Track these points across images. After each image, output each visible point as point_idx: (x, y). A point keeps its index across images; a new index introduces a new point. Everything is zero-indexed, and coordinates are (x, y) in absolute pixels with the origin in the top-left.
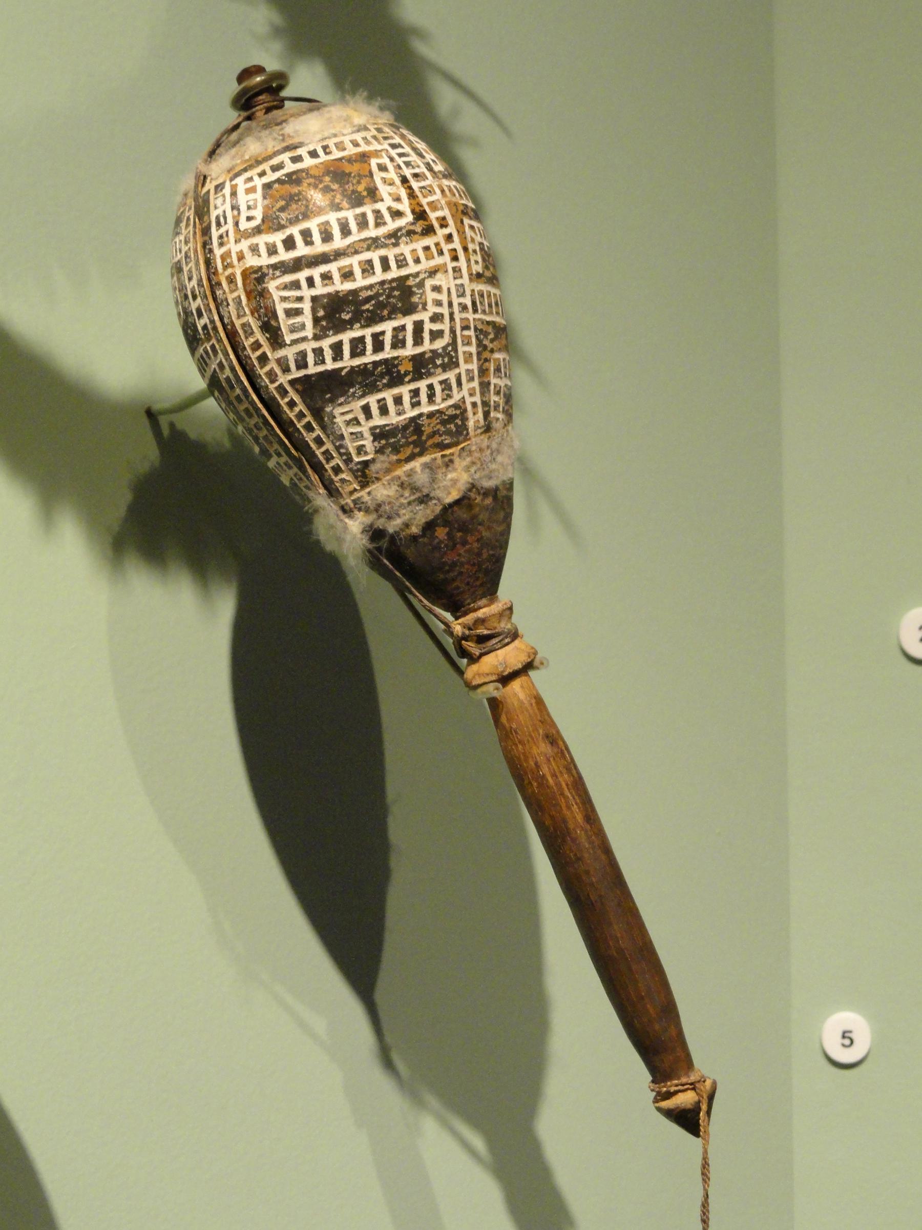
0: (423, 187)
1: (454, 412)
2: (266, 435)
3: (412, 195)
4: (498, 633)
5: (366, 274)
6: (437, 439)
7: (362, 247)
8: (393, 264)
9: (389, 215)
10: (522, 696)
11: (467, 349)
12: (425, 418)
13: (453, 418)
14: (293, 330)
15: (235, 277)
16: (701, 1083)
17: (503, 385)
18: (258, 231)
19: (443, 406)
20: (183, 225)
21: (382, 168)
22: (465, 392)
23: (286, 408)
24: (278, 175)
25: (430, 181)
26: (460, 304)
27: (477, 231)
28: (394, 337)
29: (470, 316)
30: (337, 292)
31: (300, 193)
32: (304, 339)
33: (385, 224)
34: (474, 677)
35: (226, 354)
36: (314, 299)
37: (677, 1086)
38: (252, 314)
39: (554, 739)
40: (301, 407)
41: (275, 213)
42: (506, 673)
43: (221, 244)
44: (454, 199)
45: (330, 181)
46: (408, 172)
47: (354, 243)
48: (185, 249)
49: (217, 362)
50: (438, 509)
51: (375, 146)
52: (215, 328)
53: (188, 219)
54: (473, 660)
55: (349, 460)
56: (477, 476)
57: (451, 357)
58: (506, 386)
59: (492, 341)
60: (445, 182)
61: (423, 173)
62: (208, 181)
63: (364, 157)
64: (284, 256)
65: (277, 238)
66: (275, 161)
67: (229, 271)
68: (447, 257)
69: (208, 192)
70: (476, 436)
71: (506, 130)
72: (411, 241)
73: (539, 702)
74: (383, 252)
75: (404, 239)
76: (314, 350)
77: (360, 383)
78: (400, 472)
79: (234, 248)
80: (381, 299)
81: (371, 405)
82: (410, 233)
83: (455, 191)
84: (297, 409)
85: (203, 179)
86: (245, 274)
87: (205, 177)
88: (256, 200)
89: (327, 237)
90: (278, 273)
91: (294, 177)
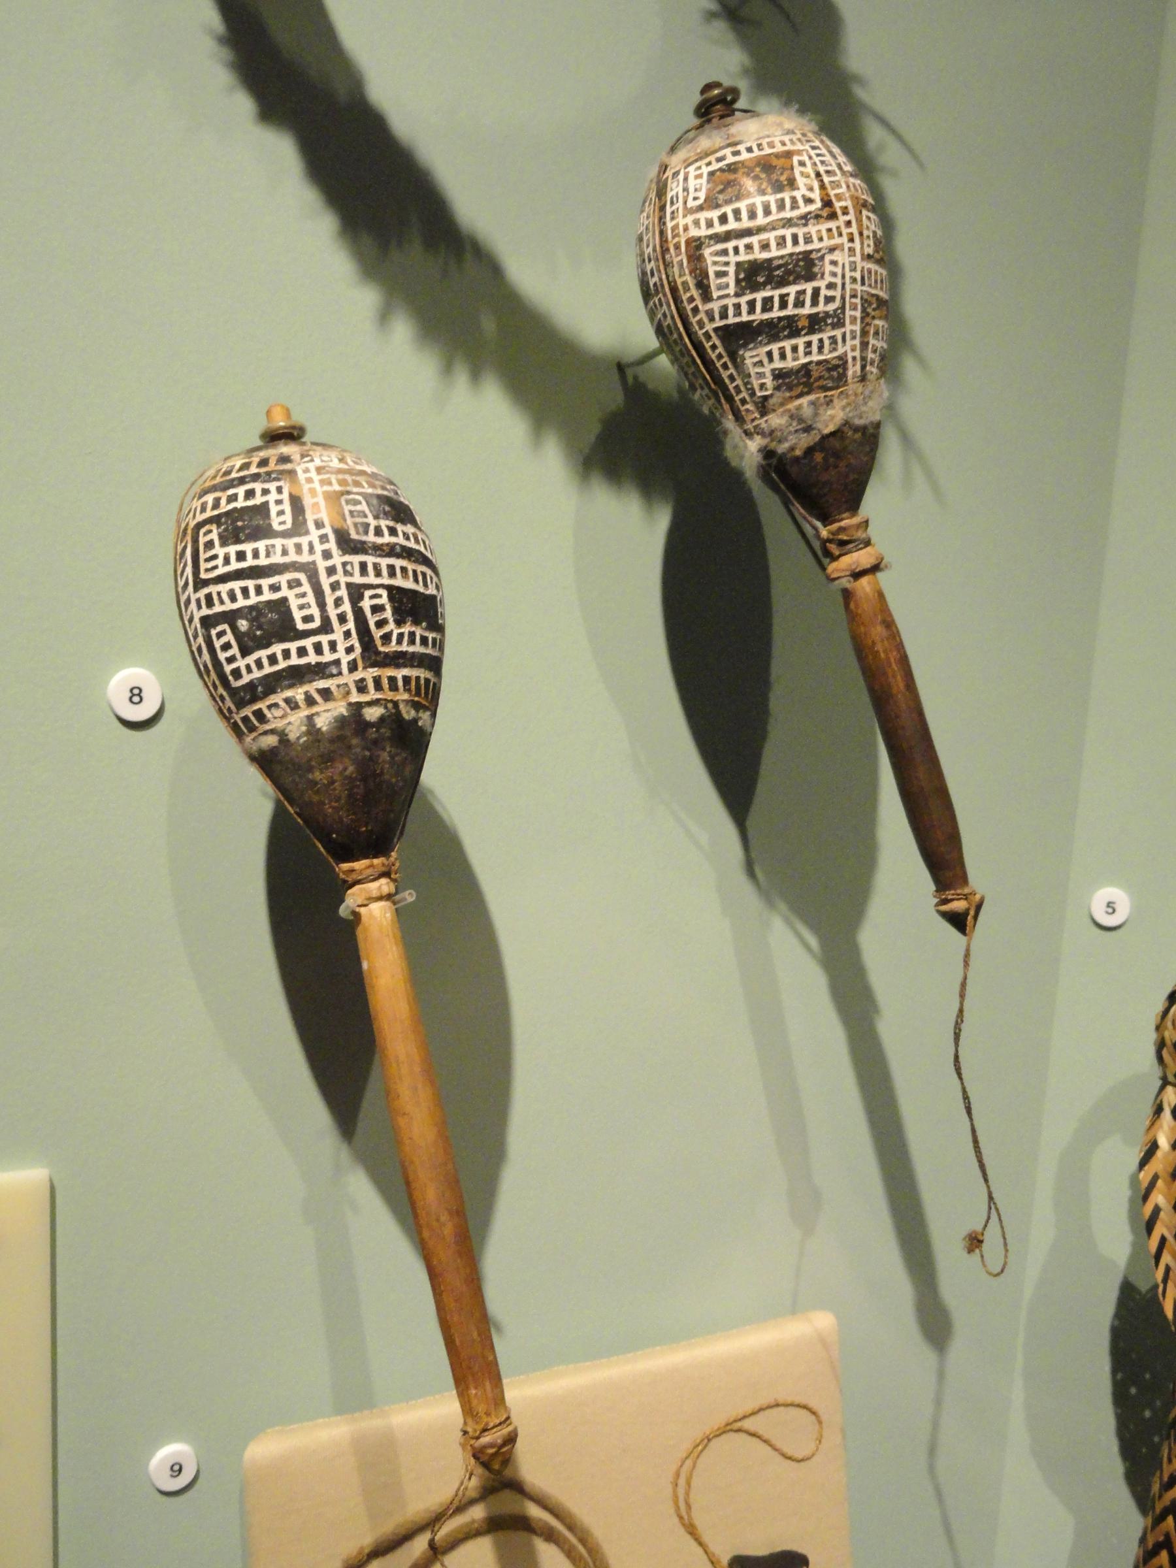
0: (833, 182)
1: (837, 362)
2: (694, 372)
3: (823, 187)
4: (855, 540)
5: (779, 246)
6: (821, 383)
7: (778, 225)
8: (801, 240)
9: (802, 201)
10: (868, 589)
11: (853, 313)
12: (814, 364)
13: (836, 367)
14: (720, 288)
15: (680, 245)
16: (973, 896)
17: (879, 346)
18: (701, 208)
19: (829, 356)
20: (647, 204)
21: (802, 164)
22: (848, 347)
23: (709, 351)
24: (721, 165)
25: (839, 176)
26: (851, 277)
27: (873, 221)
28: (797, 298)
29: (858, 287)
30: (756, 260)
31: (735, 180)
32: (727, 296)
33: (798, 208)
34: (833, 572)
35: (669, 306)
36: (738, 264)
37: (953, 895)
38: (691, 273)
39: (889, 624)
40: (720, 350)
41: (714, 194)
42: (857, 570)
43: (673, 218)
44: (856, 194)
45: (760, 171)
46: (822, 169)
47: (773, 221)
48: (646, 223)
49: (663, 311)
50: (818, 438)
51: (799, 147)
52: (662, 285)
53: (651, 199)
54: (835, 558)
55: (753, 394)
56: (851, 415)
57: (839, 319)
58: (882, 347)
59: (874, 310)
60: (852, 180)
61: (834, 171)
62: (668, 169)
63: (788, 155)
64: (719, 229)
65: (715, 214)
66: (719, 154)
67: (676, 240)
68: (845, 239)
69: (667, 178)
70: (854, 383)
71: (921, 165)
72: (818, 223)
73: (881, 595)
74: (794, 230)
75: (812, 221)
76: (734, 305)
77: (767, 333)
78: (791, 406)
79: (682, 222)
80: (789, 267)
81: (773, 351)
82: (817, 217)
83: (859, 188)
84: (717, 351)
85: (664, 168)
86: (688, 242)
87: (666, 167)
88: (701, 184)
89: (752, 215)
90: (712, 242)
91: (732, 167)
